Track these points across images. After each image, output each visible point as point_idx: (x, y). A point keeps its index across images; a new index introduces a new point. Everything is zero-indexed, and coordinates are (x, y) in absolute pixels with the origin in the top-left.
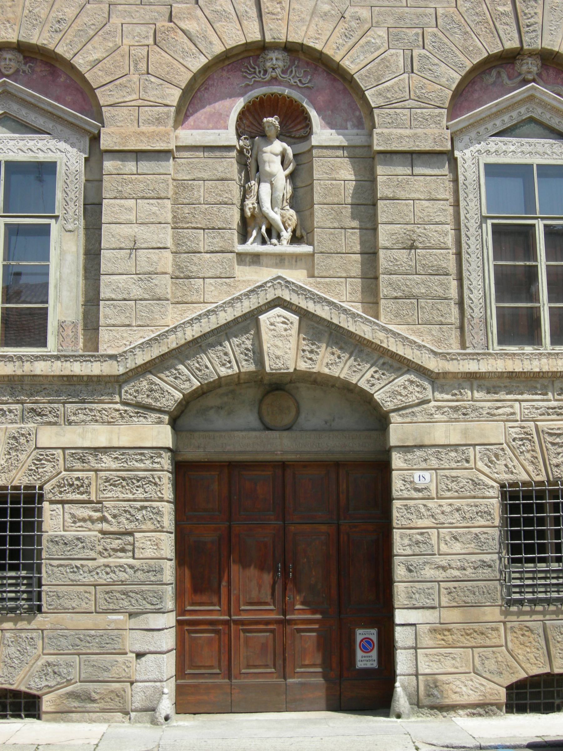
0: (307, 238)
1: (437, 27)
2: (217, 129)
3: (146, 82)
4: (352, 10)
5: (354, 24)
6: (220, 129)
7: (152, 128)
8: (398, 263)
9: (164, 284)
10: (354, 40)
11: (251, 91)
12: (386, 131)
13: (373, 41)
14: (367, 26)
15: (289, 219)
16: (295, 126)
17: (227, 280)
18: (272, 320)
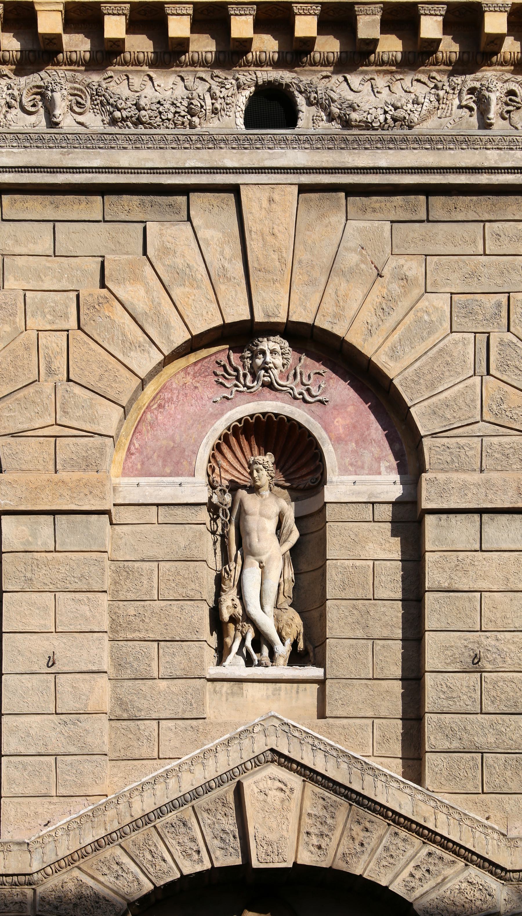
0: (314, 655)
2: (178, 475)
3: (67, 396)
4: (393, 262)
5: (396, 288)
6: (182, 475)
7: (77, 475)
8: (454, 695)
9: (100, 733)
10: (395, 317)
11: (231, 409)
12: (441, 476)
15: (287, 624)
16: (299, 469)
17: (194, 723)
18: (261, 786)
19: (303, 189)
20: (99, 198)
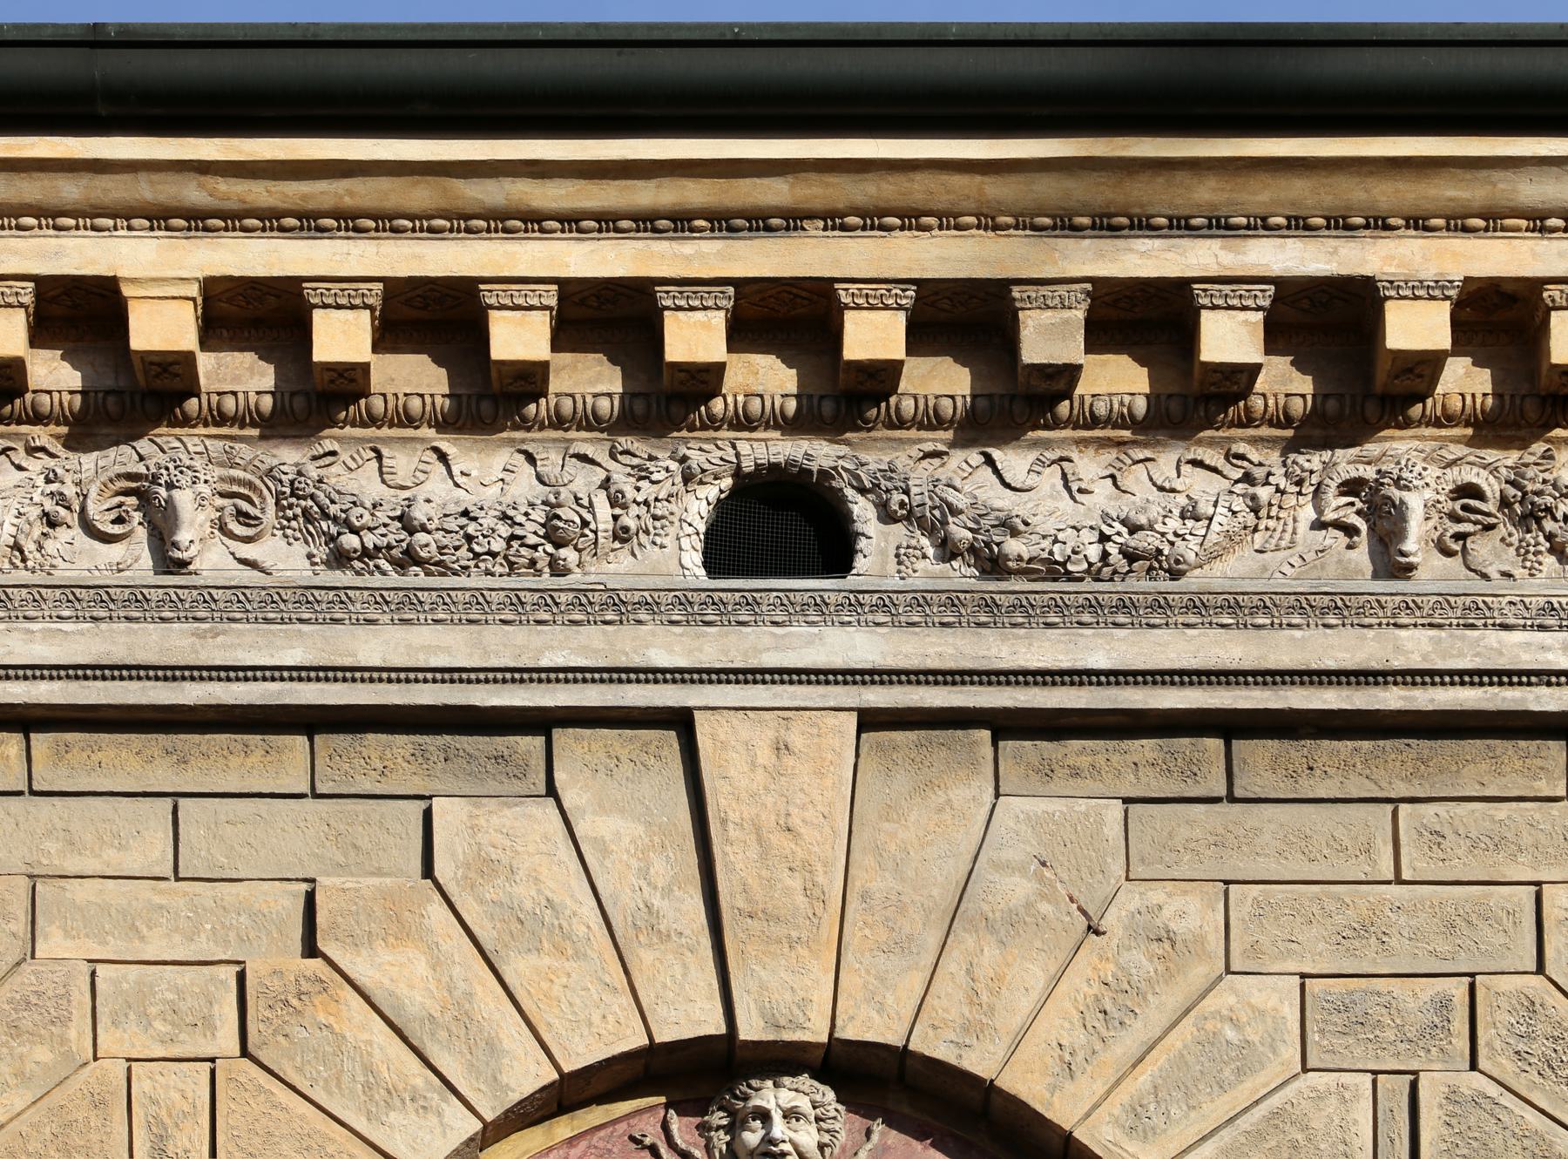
1: (1540, 969)
4: (1131, 900)
5: (1140, 961)
13: (1230, 1033)
14: (1200, 973)
19: (870, 721)
20: (301, 741)
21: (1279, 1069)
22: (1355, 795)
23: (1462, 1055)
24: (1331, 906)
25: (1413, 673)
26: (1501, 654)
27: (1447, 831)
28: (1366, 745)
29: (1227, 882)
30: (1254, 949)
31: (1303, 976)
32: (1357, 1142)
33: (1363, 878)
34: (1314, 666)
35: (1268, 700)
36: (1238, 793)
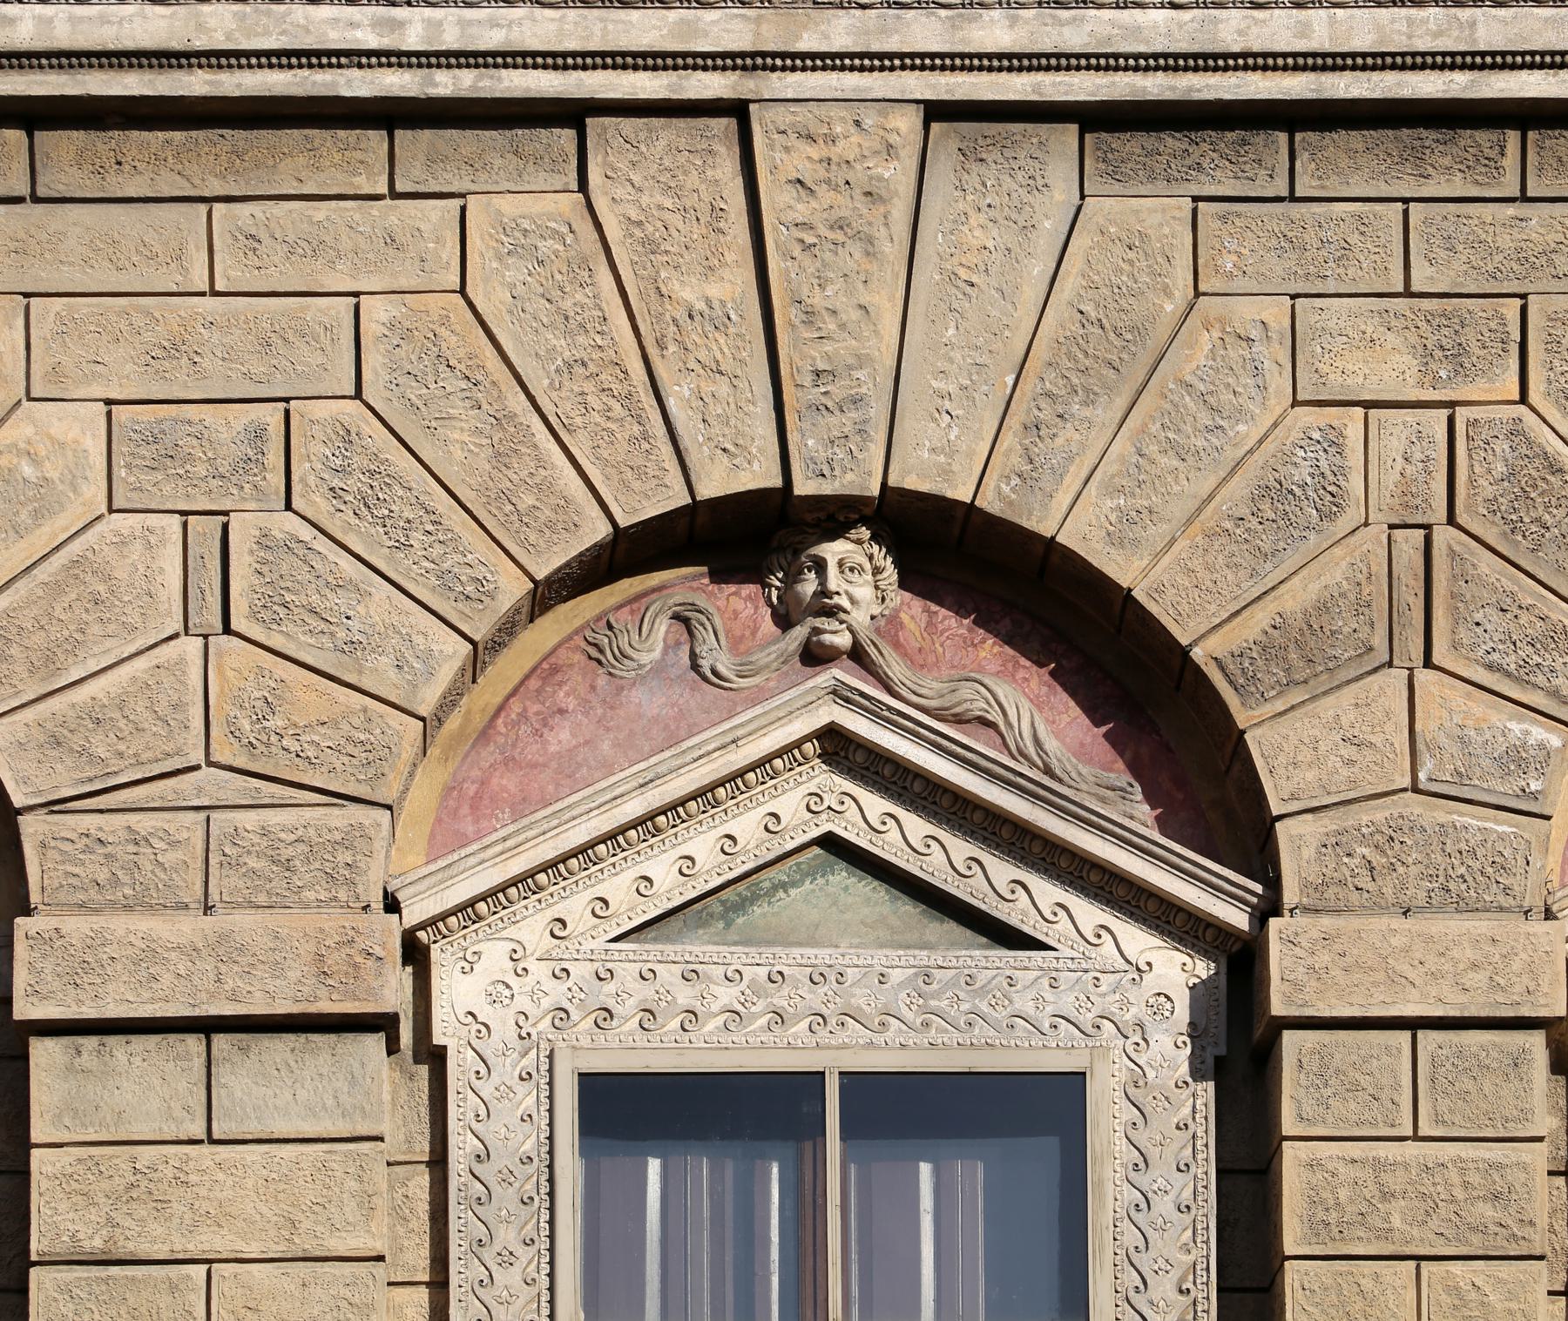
1: (358, 395)
12: (77, 926)
13: (27, 470)
19: (936, 112)
20: (1282, 137)
21: (80, 510)
22: (167, 194)
23: (277, 493)
24: (139, 321)
25: (218, 54)
26: (308, 31)
27: (263, 235)
28: (178, 136)
29: (26, 295)
30: (56, 371)
31: (109, 402)
32: (163, 595)
33: (175, 289)
34: (111, 47)
35: (64, 85)
36: (42, 192)
